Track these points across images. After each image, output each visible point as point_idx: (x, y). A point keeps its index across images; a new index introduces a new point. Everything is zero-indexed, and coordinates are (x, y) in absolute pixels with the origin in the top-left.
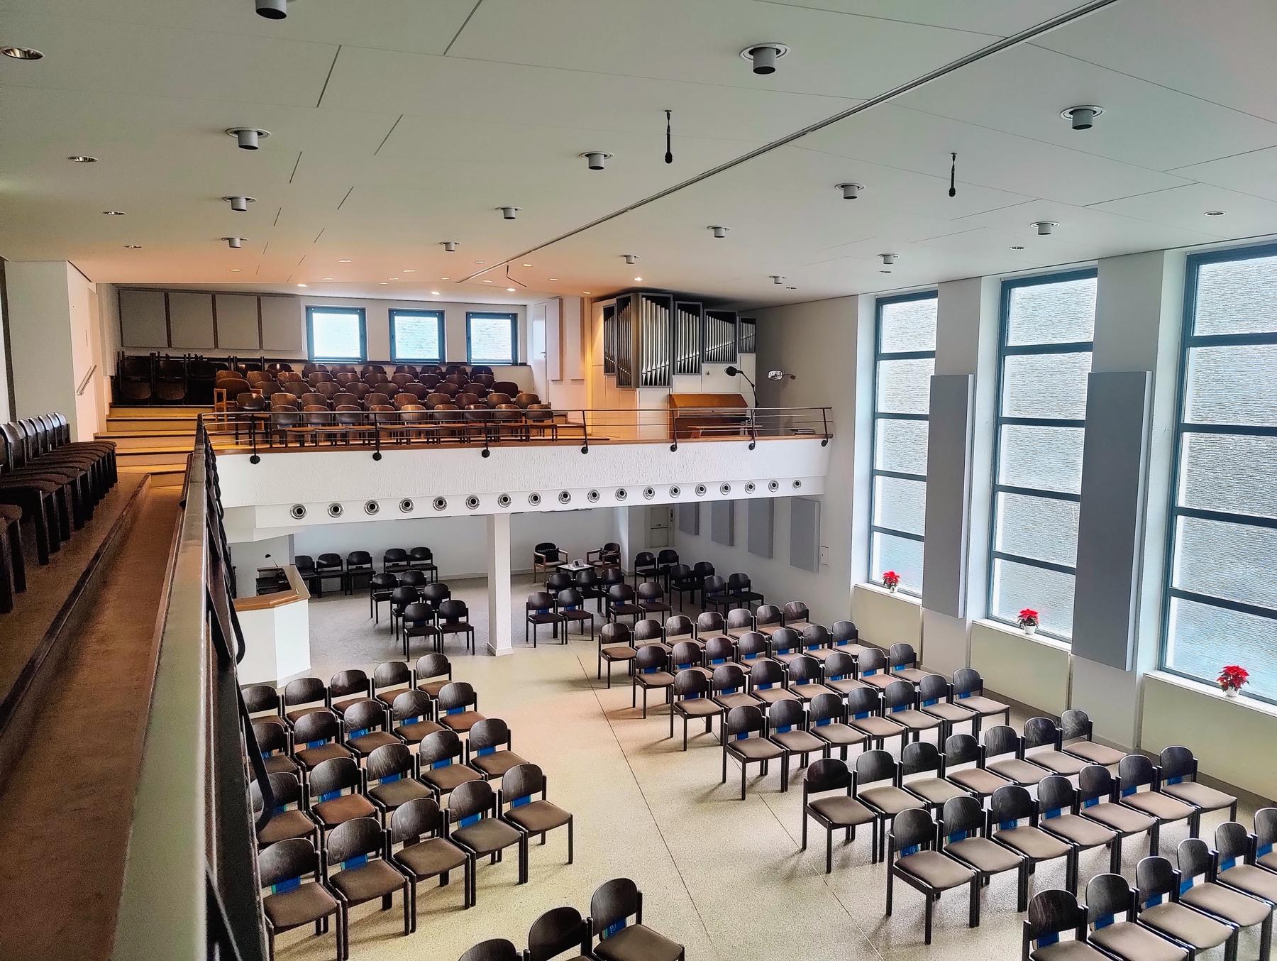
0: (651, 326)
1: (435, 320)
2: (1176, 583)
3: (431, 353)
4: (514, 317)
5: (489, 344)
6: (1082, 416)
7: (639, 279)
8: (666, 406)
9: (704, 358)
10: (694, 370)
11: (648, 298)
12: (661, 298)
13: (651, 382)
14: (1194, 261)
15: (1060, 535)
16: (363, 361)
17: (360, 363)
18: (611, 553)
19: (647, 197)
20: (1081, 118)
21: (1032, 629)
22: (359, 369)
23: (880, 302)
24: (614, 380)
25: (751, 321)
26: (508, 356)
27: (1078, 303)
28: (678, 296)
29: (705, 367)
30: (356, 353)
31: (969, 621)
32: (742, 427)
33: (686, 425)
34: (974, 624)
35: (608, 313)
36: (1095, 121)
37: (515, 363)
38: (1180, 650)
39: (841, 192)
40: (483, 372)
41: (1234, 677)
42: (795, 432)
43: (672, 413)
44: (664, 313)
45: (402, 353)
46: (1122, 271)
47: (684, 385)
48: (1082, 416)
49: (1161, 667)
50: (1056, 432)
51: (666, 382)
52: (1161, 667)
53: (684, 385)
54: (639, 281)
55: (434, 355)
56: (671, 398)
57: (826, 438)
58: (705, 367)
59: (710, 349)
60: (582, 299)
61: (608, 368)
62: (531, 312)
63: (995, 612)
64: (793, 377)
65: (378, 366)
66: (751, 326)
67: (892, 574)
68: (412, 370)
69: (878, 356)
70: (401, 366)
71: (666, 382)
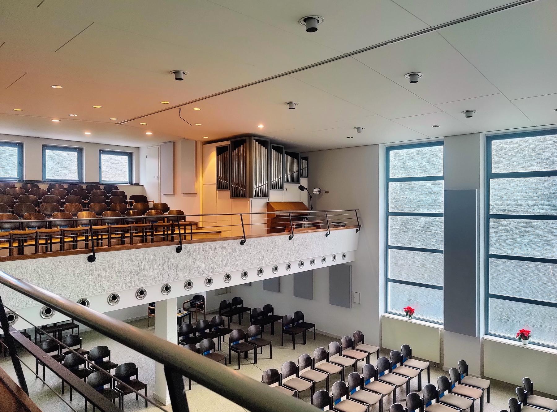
0: (258, 157)
1: (75, 154)
2: (389, 277)
3: (72, 175)
4: (130, 155)
5: (113, 171)
6: (442, 212)
7: (261, 126)
8: (265, 210)
9: (284, 180)
10: (279, 187)
11: (257, 141)
12: (264, 142)
13: (257, 195)
14: (489, 139)
15: (434, 269)
16: (20, 180)
17: (19, 182)
18: (199, 302)
19: (196, 98)
20: (413, 77)
21: (527, 341)
22: (18, 186)
23: (388, 149)
24: (228, 193)
25: (306, 159)
26: (126, 179)
27: (434, 158)
28: (272, 141)
29: (286, 185)
30: (15, 174)
31: (380, 315)
32: (305, 222)
33: (280, 223)
34: (383, 317)
35: (220, 151)
36: (419, 79)
37: (131, 184)
38: (497, 326)
39: (288, 106)
40: (111, 189)
41: (524, 335)
42: (338, 225)
43: (268, 215)
44: (265, 151)
45: (50, 176)
46: (458, 144)
47: (275, 197)
48: (442, 212)
49: (387, 312)
50: (500, 221)
51: (265, 194)
52: (387, 312)
53: (275, 197)
54: (261, 128)
55: (74, 177)
56: (268, 205)
57: (358, 227)
58: (286, 185)
59: (288, 175)
60: (196, 142)
61: (221, 186)
62: (143, 153)
63: (390, 310)
64: (327, 192)
65: (34, 184)
66: (305, 162)
67: (409, 308)
68: (61, 186)
69: (388, 179)
70: (52, 184)
71: (265, 194)
